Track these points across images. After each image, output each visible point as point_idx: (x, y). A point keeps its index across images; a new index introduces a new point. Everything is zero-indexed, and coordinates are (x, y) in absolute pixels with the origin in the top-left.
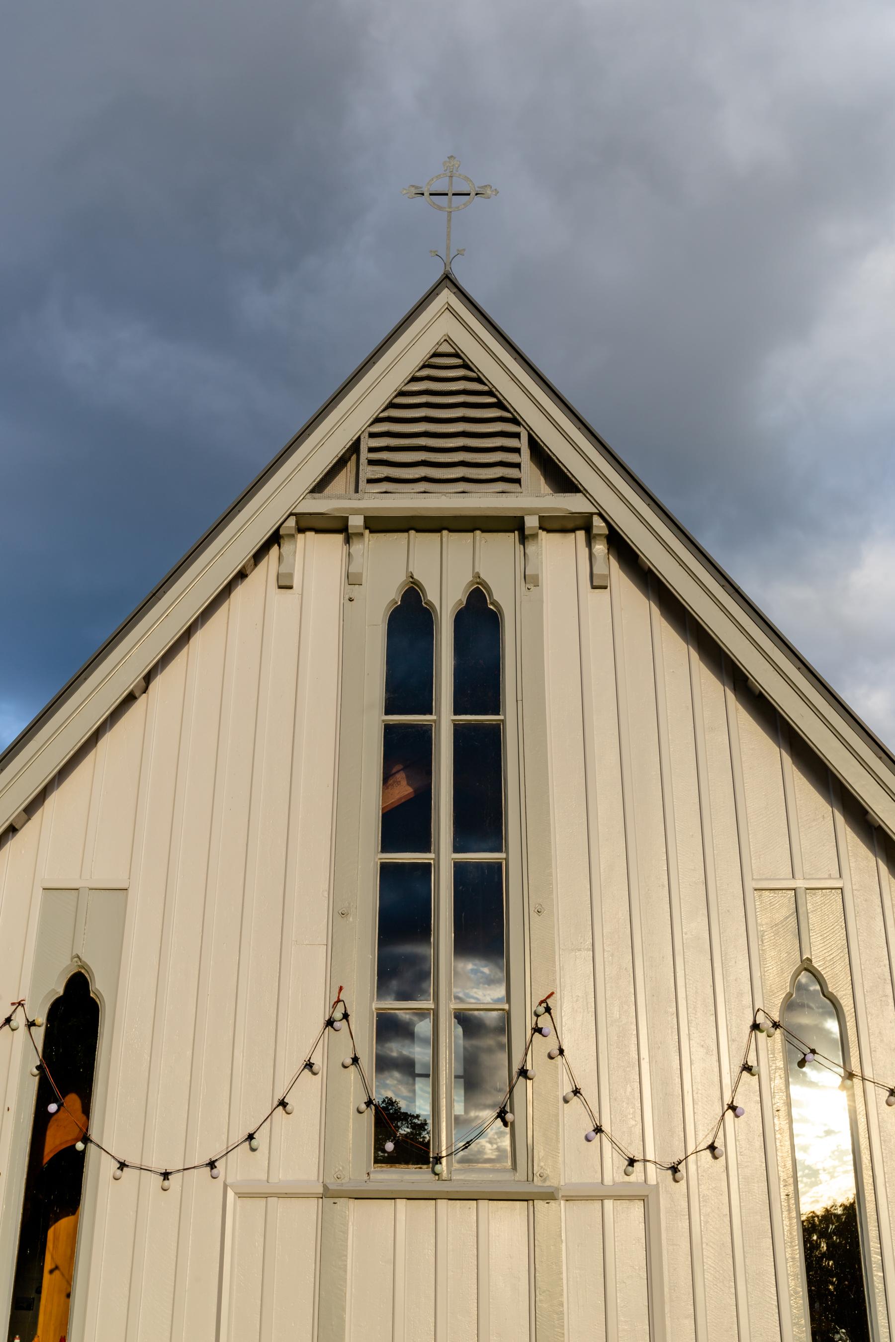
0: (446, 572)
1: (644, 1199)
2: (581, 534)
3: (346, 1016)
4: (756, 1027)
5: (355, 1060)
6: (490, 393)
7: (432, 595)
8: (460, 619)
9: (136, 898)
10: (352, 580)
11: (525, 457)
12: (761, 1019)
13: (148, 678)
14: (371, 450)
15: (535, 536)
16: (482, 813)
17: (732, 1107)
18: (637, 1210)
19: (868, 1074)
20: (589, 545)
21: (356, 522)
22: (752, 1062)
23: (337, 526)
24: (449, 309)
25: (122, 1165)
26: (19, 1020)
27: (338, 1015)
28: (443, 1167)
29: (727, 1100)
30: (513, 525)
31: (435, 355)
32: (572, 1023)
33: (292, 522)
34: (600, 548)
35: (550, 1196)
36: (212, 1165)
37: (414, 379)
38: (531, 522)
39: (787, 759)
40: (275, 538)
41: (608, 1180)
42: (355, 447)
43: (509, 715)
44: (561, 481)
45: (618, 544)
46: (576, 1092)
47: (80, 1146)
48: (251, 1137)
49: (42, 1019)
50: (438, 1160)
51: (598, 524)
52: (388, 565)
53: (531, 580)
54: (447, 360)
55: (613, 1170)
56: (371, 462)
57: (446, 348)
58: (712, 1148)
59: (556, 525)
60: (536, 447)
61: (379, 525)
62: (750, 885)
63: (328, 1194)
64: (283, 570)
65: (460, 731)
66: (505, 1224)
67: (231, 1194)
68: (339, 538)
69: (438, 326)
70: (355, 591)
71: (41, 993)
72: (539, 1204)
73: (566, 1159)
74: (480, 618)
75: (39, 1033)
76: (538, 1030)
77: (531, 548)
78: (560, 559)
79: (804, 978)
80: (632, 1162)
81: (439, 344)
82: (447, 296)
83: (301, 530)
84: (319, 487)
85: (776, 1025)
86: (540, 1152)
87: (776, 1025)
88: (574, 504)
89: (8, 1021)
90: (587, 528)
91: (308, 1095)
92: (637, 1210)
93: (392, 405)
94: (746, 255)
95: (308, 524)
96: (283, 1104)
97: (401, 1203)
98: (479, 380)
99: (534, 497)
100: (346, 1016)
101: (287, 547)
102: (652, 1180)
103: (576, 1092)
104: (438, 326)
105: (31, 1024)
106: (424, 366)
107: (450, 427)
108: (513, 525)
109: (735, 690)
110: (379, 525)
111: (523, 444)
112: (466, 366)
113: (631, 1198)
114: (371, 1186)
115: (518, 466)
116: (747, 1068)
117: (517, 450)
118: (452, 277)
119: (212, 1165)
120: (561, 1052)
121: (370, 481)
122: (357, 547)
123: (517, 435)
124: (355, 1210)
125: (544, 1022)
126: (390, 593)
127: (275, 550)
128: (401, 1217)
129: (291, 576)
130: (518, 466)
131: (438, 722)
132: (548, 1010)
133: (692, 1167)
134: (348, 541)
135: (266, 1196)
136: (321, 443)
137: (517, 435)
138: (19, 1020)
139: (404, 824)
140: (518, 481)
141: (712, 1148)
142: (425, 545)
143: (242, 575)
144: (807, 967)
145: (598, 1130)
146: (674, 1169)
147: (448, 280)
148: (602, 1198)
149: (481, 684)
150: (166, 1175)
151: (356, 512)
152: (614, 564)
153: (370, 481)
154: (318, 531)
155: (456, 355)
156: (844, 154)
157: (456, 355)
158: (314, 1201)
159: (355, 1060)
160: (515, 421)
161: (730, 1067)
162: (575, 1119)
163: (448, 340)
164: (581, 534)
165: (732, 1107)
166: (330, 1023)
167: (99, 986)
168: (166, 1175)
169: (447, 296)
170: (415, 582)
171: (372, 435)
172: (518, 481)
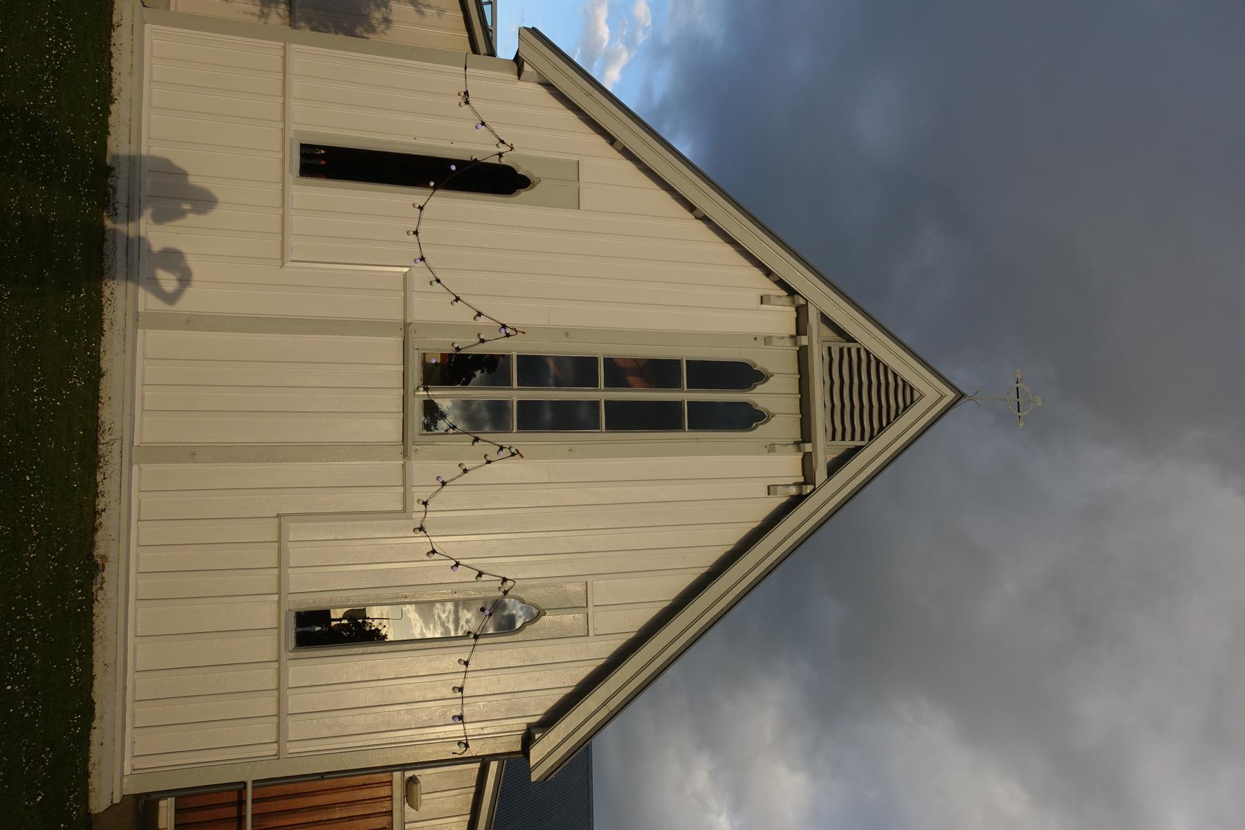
0: (774, 396)
1: (404, 510)
2: (802, 479)
3: (508, 335)
4: (505, 580)
5: (482, 341)
6: (889, 423)
7: (760, 388)
8: (746, 406)
9: (574, 214)
10: (768, 340)
11: (849, 444)
12: (509, 583)
13: (705, 219)
14: (849, 350)
15: (799, 450)
16: (627, 418)
17: (457, 564)
18: (399, 507)
19: (468, 675)
20: (795, 484)
21: (804, 340)
22: (484, 577)
23: (801, 326)
24: (942, 397)
25: (421, 208)
26: (503, 148)
27: (508, 331)
28: (422, 393)
29: (461, 562)
30: (806, 434)
31: (912, 389)
32: (506, 469)
33: (802, 302)
34: (794, 491)
35: (405, 454)
36: (422, 259)
37: (895, 376)
38: (808, 447)
39: (666, 604)
40: (791, 292)
41: (414, 489)
42: (851, 339)
43: (687, 435)
44: (834, 468)
45: (796, 502)
46: (465, 471)
47: (432, 184)
48: (438, 281)
49: (504, 161)
50: (426, 389)
51: (809, 488)
52: (779, 363)
53: (771, 449)
54: (909, 396)
55: (420, 493)
56: (841, 350)
57: (916, 395)
58: (434, 552)
59: (807, 463)
60: (855, 451)
61: (803, 356)
62: (589, 579)
63: (406, 326)
64: (772, 299)
65: (678, 405)
66: (390, 429)
67: (406, 270)
68: (794, 333)
69: (931, 393)
70: (761, 342)
71: (519, 159)
72: (401, 449)
73: (430, 464)
74: (746, 418)
75: (495, 160)
76: (501, 448)
77: (792, 448)
78: (787, 467)
79: (535, 611)
80: (425, 503)
81: (919, 391)
82: (950, 395)
83: (797, 309)
84: (825, 319)
85: (506, 593)
86: (430, 449)
87: (506, 593)
88: (821, 474)
89: (502, 142)
90: (805, 483)
91: (461, 314)
92: (399, 507)
93: (878, 362)
94: (1008, 702)
95: (801, 313)
96: (457, 299)
97: (401, 368)
98: (897, 415)
99: (824, 451)
100: (508, 335)
101: (787, 300)
102: (414, 516)
103: (465, 471)
104: (931, 393)
105: (500, 155)
106: (904, 381)
107: (863, 398)
108: (806, 434)
109: (707, 573)
110: (803, 356)
111: (858, 443)
112: (905, 408)
113: (404, 502)
114: (411, 351)
115: (843, 439)
116: (480, 574)
117: (853, 439)
118: (963, 400)
119: (422, 259)
120: (489, 462)
121: (829, 349)
122: (788, 343)
123: (862, 439)
124: (396, 341)
125: (506, 452)
126: (761, 363)
127: (784, 293)
128: (394, 368)
129: (769, 303)
130: (843, 439)
131: (683, 391)
132: (513, 454)
133: (422, 540)
134: (792, 337)
135: (405, 290)
136: (852, 319)
137: (862, 439)
138: (503, 148)
139: (619, 372)
140: (833, 439)
141: (434, 552)
142: (792, 385)
143: (768, 273)
144: (541, 613)
145: (444, 484)
146: (421, 529)
147: (961, 396)
148: (404, 485)
149: (707, 418)
150: (416, 233)
151: (810, 340)
152: (784, 500)
153: (829, 349)
154: (797, 319)
155: (912, 402)
156: (1088, 778)
157: (912, 402)
158: (400, 317)
159: (482, 341)
160: (872, 438)
161: (481, 564)
162: (449, 469)
163: (922, 396)
164: (802, 479)
165: (457, 564)
166: (504, 326)
167: (524, 194)
168: (416, 233)
169: (950, 395)
170: (767, 379)
171: (858, 350)
172: (833, 439)
